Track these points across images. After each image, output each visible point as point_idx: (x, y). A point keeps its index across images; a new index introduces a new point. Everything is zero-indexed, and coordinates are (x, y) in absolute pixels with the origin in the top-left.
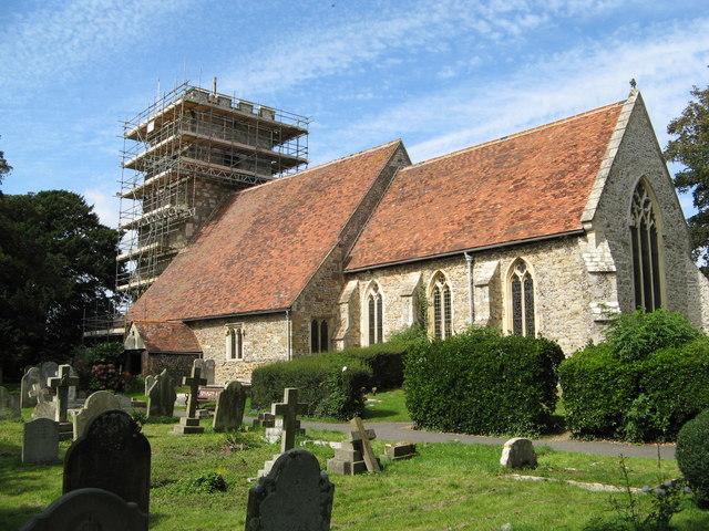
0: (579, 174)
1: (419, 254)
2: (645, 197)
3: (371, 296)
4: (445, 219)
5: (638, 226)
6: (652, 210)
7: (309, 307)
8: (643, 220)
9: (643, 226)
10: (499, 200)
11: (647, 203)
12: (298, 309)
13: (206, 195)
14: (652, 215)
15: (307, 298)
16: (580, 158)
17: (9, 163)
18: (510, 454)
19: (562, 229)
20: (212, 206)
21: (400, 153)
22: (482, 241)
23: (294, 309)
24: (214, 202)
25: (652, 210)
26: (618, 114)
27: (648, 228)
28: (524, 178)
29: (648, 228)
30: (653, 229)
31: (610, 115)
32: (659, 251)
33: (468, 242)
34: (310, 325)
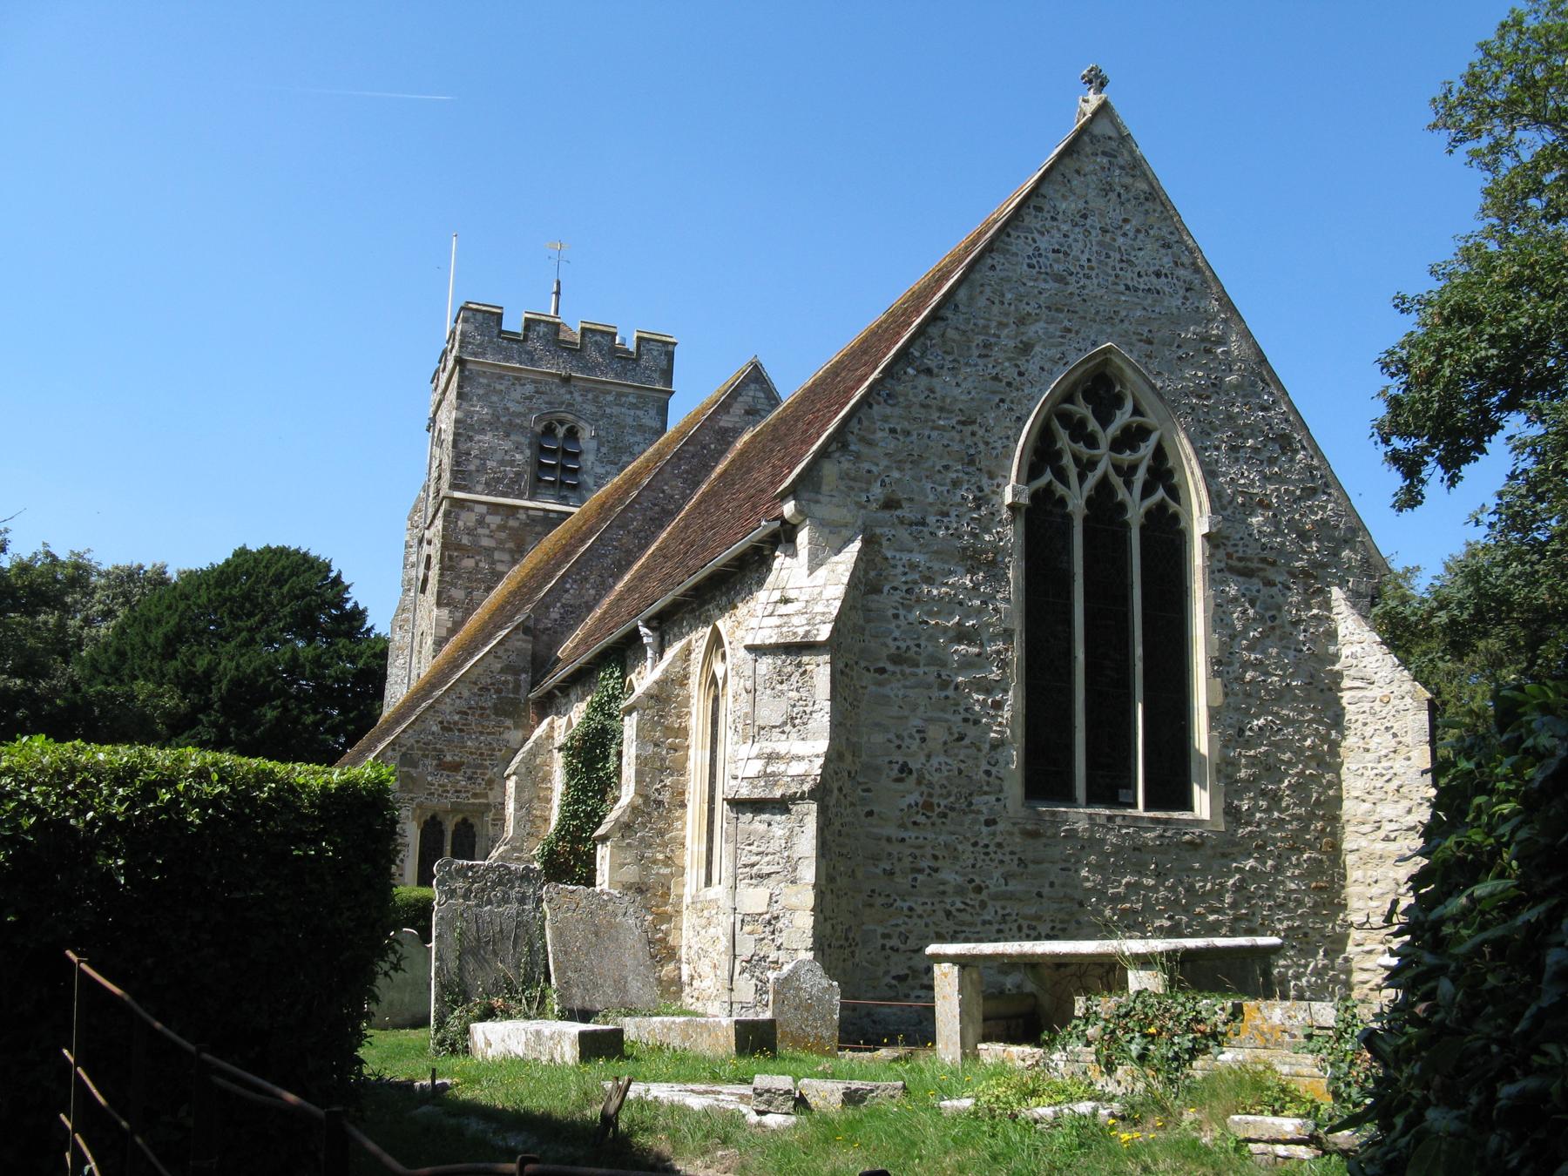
9: (1104, 505)
13: (486, 542)
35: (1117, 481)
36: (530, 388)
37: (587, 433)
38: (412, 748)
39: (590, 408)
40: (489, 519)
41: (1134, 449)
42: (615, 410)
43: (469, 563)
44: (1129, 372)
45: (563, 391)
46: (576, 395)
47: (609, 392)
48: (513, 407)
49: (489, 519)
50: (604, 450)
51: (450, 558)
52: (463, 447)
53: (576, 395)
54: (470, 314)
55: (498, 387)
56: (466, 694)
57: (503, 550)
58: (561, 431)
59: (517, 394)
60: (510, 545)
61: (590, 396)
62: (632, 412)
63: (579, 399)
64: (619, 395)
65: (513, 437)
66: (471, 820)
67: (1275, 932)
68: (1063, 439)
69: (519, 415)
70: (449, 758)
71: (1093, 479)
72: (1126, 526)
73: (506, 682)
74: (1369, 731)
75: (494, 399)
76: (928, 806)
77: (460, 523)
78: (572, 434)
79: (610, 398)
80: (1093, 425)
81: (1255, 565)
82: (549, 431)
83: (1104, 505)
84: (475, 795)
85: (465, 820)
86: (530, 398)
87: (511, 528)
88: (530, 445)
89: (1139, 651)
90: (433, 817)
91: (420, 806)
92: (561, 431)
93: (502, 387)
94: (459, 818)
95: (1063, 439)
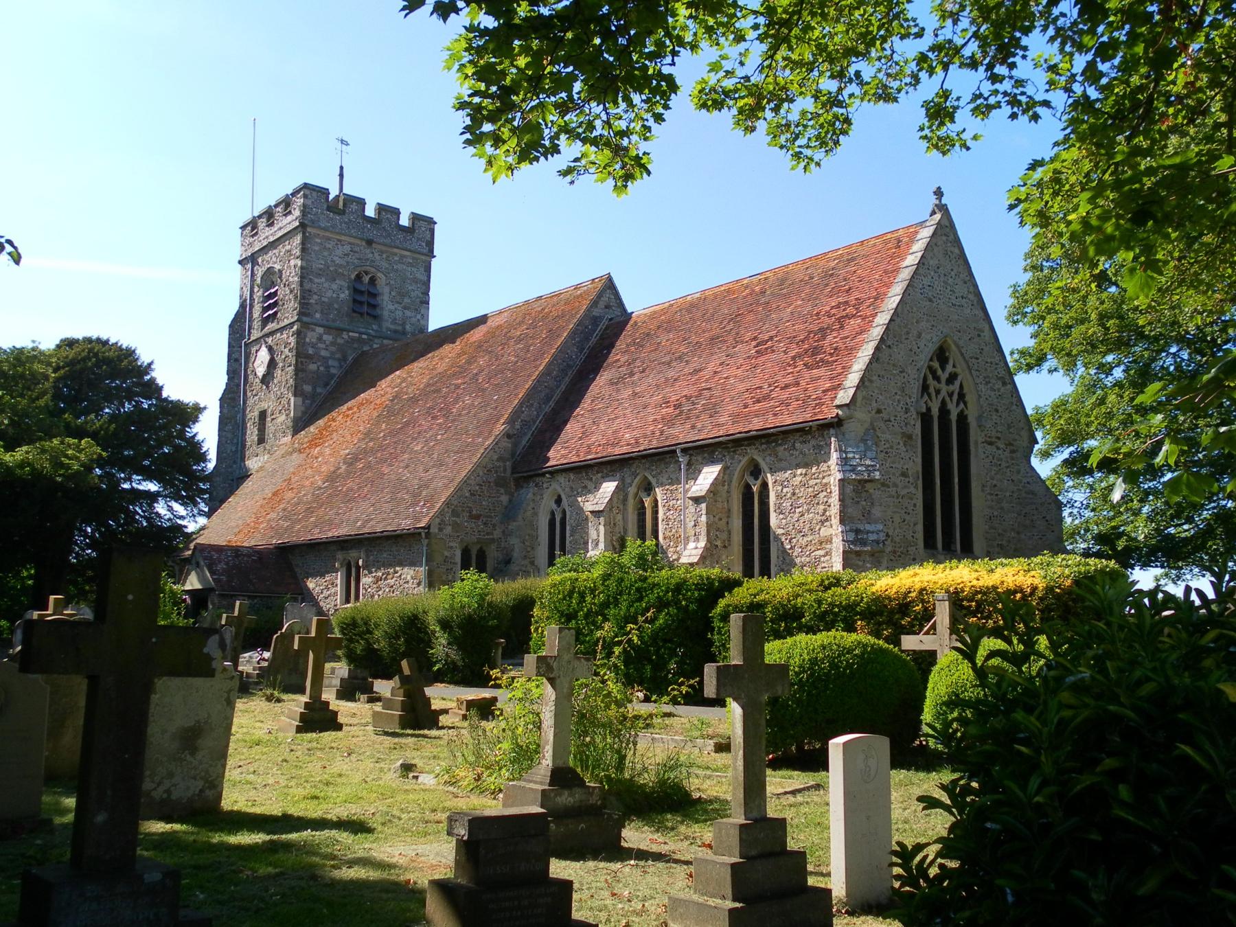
0: (845, 333)
1: (617, 451)
2: (949, 368)
3: (553, 514)
4: (658, 398)
5: (935, 412)
6: (961, 386)
7: (456, 526)
8: (943, 403)
9: (944, 412)
10: (733, 371)
11: (952, 378)
12: (440, 530)
13: (323, 353)
14: (962, 396)
15: (455, 513)
16: (850, 310)
17: (956, 120)
18: (922, 710)
19: (808, 417)
20: (333, 371)
21: (608, 293)
22: (707, 431)
23: (434, 530)
24: (336, 364)
25: (961, 386)
26: (909, 245)
27: (954, 417)
28: (771, 338)
29: (954, 417)
30: (962, 418)
31: (897, 244)
32: (82, 702)
33: (682, 434)
34: (458, 553)
35: (948, 399)
36: (347, 248)
37: (381, 279)
38: (456, 506)
39: (385, 265)
40: (325, 337)
41: (953, 384)
42: (399, 267)
43: (313, 367)
44: (953, 347)
45: (368, 251)
46: (376, 255)
47: (396, 254)
48: (338, 261)
49: (325, 337)
50: (393, 294)
51: (302, 362)
52: (307, 286)
53: (376, 255)
54: (308, 192)
55: (328, 246)
56: (481, 474)
57: (334, 359)
58: (366, 279)
59: (339, 252)
60: (338, 356)
61: (384, 256)
62: (409, 269)
63: (378, 258)
64: (402, 257)
65: (337, 281)
66: (484, 548)
67: (1170, 609)
68: (931, 381)
69: (341, 266)
70: (474, 512)
71: (940, 397)
72: (950, 420)
73: (500, 467)
74: (1035, 518)
75: (326, 254)
76: (895, 552)
77: (307, 340)
78: (373, 281)
79: (396, 258)
80: (939, 372)
81: (994, 440)
82: (359, 277)
83: (944, 412)
84: (488, 534)
85: (481, 548)
86: (347, 255)
87: (339, 344)
88: (348, 288)
89: (956, 480)
90: (466, 547)
91: (462, 540)
92: (366, 279)
93: (330, 246)
94: (479, 546)
95: (931, 381)
